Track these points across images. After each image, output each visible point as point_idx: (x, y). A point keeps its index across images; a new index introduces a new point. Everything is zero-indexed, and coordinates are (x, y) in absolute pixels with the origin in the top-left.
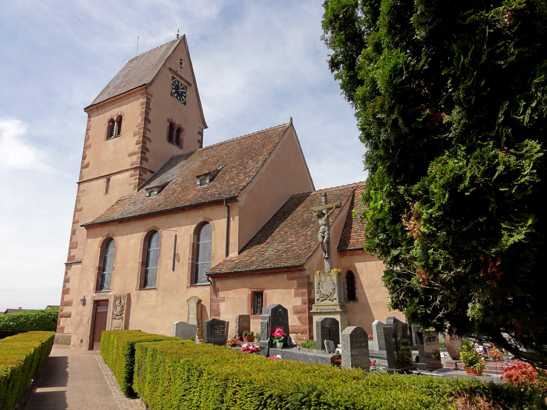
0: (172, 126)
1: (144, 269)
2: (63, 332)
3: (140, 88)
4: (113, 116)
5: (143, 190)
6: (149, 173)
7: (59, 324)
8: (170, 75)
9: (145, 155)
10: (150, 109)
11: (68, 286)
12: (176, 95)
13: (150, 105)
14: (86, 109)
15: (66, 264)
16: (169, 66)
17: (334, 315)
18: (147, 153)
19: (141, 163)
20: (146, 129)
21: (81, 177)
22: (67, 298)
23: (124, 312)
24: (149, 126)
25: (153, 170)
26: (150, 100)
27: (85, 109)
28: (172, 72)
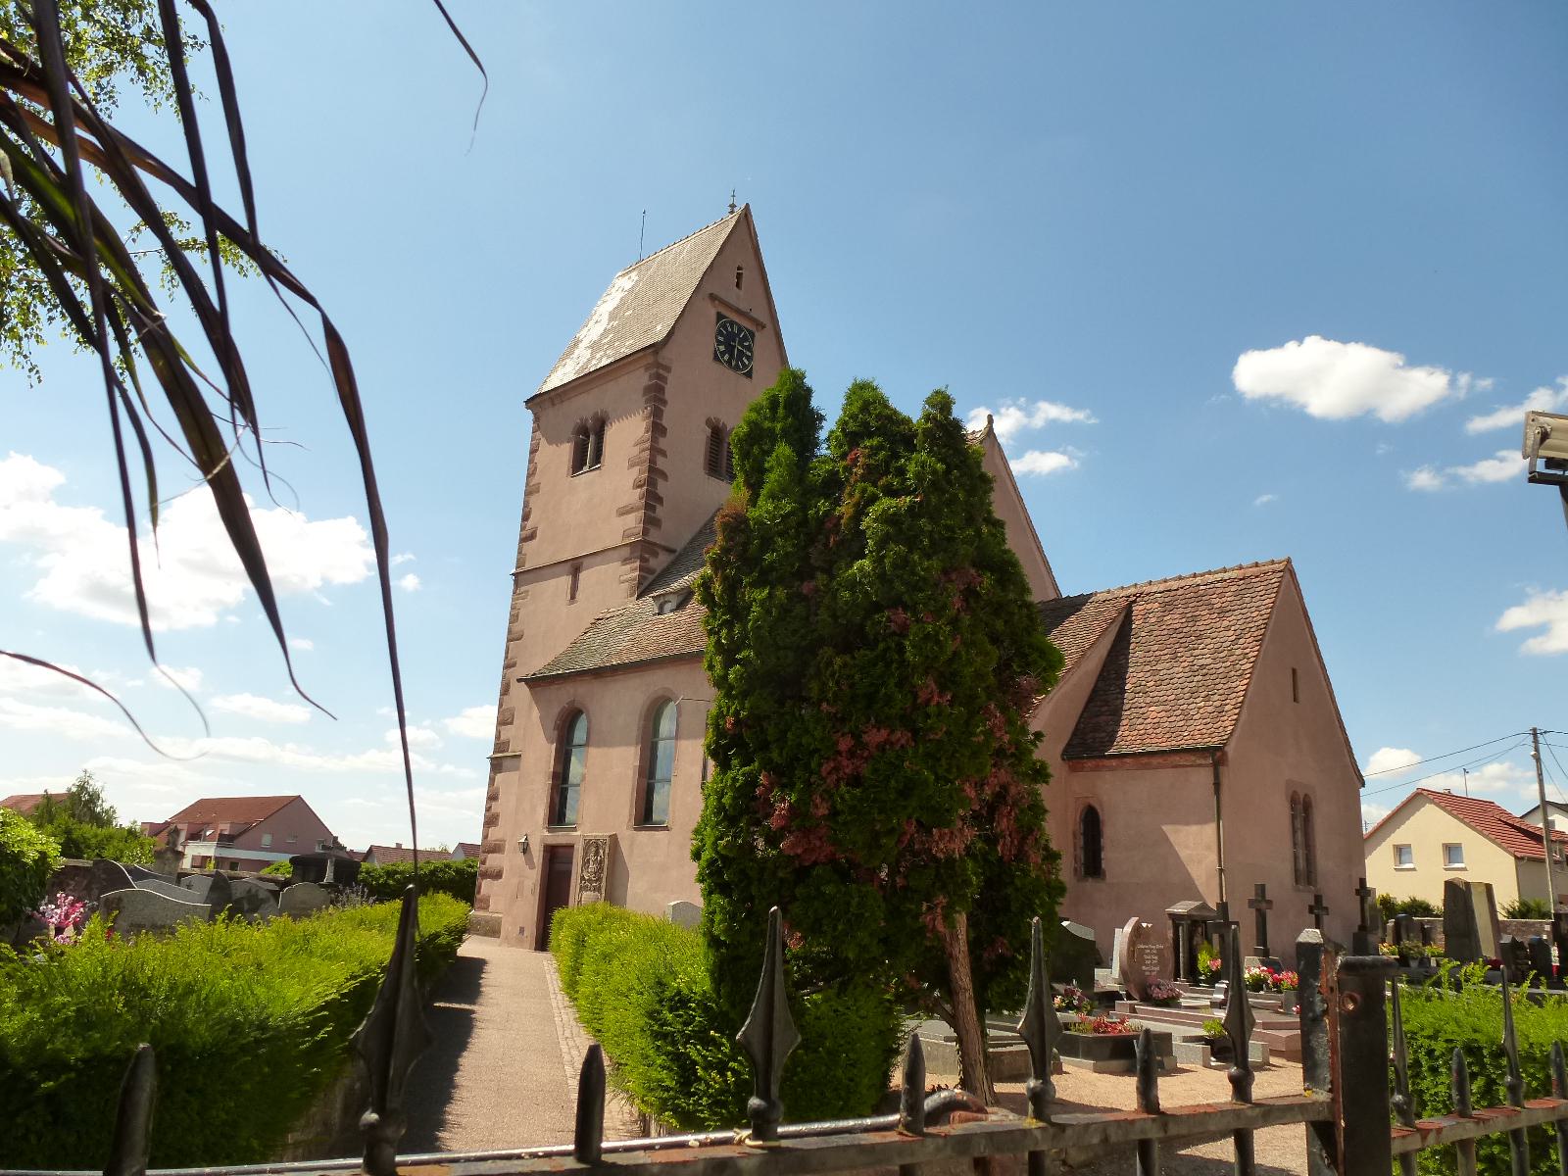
0: (717, 434)
1: (645, 782)
2: (486, 908)
3: (641, 354)
4: (587, 420)
5: (648, 599)
6: (664, 552)
7: (479, 892)
8: (713, 313)
9: (654, 512)
10: (665, 403)
11: (496, 807)
12: (726, 357)
13: (664, 393)
14: (530, 403)
15: (491, 758)
16: (708, 289)
17: (398, 932)
18: (658, 506)
19: (645, 532)
20: (655, 451)
21: (520, 563)
22: (495, 833)
23: (604, 876)
24: (663, 443)
25: (673, 546)
26: (664, 379)
27: (527, 402)
28: (717, 302)
